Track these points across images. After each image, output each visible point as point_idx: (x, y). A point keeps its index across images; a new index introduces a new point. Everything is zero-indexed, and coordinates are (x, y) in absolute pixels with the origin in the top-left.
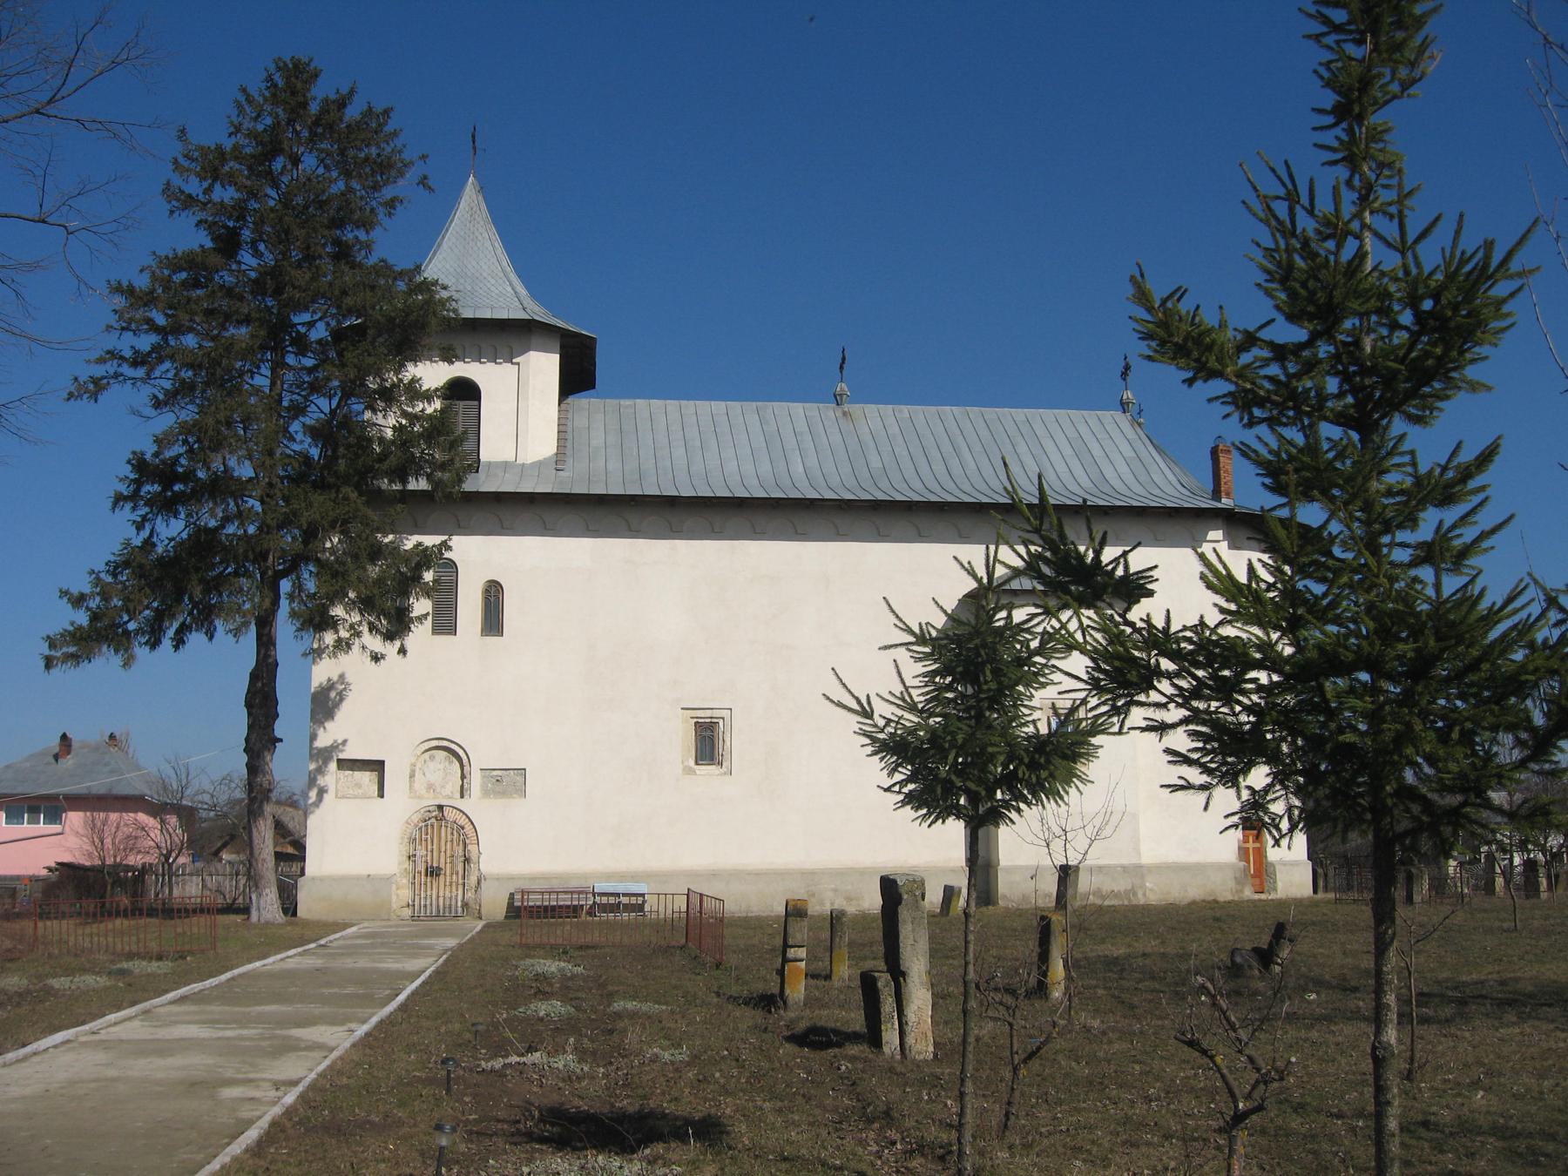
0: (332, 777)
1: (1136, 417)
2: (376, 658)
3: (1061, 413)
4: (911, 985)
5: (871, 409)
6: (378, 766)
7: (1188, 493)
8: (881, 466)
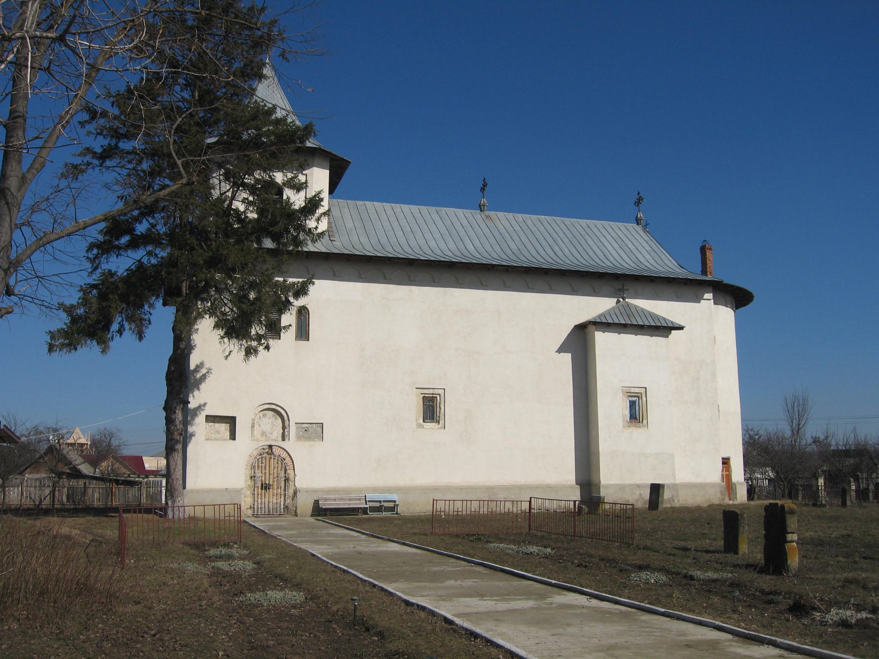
6: (231, 421)
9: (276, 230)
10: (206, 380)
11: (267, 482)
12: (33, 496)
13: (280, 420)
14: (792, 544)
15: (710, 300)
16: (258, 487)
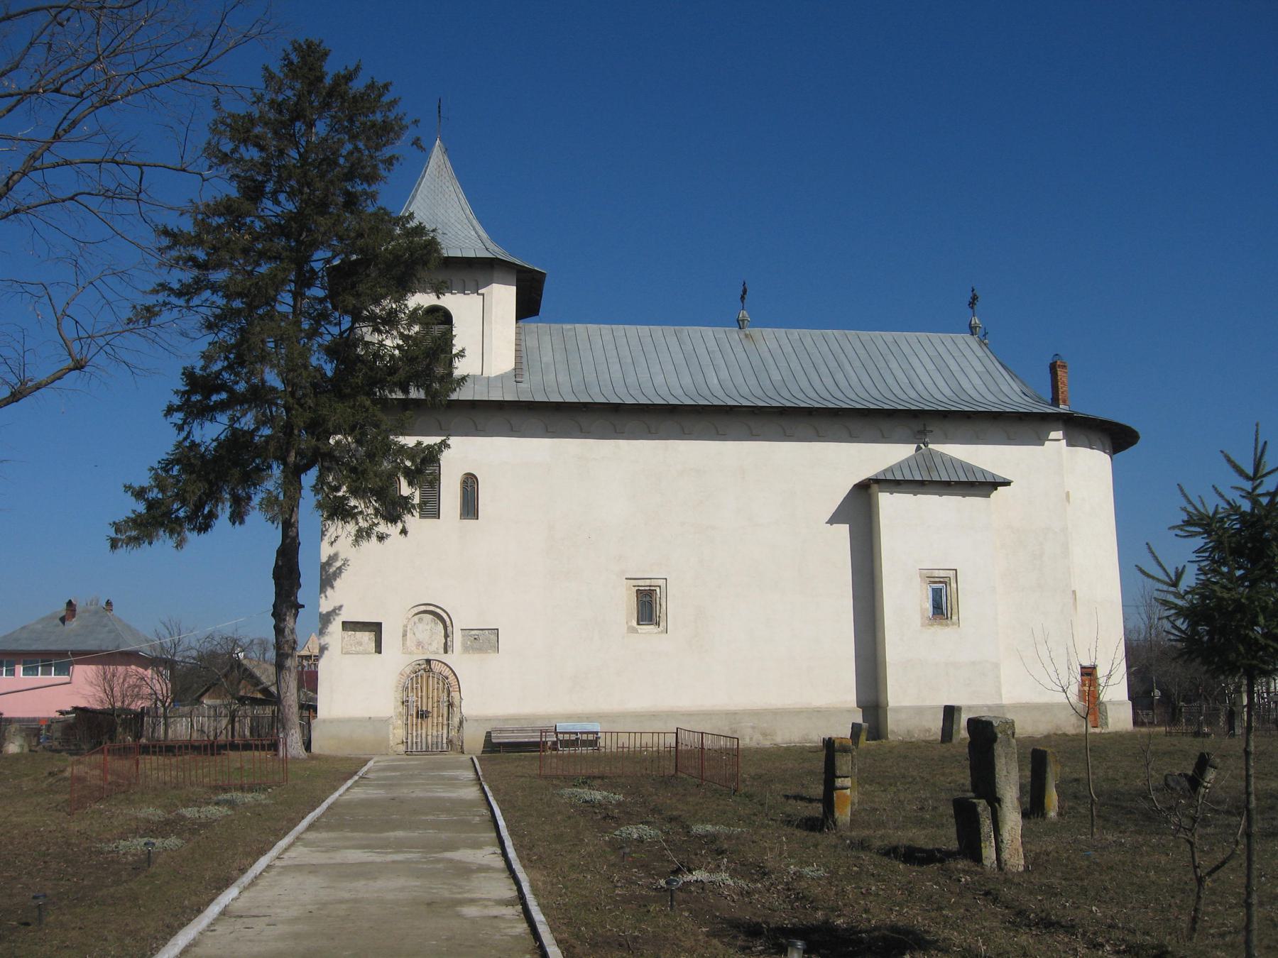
1: (983, 338)
2: (381, 538)
3: (922, 336)
5: (768, 331)
6: (376, 628)
7: (1031, 401)
8: (780, 378)
10: (343, 575)
11: (424, 709)
12: (206, 729)
13: (441, 626)
14: (845, 791)
15: (1059, 440)
16: (412, 715)
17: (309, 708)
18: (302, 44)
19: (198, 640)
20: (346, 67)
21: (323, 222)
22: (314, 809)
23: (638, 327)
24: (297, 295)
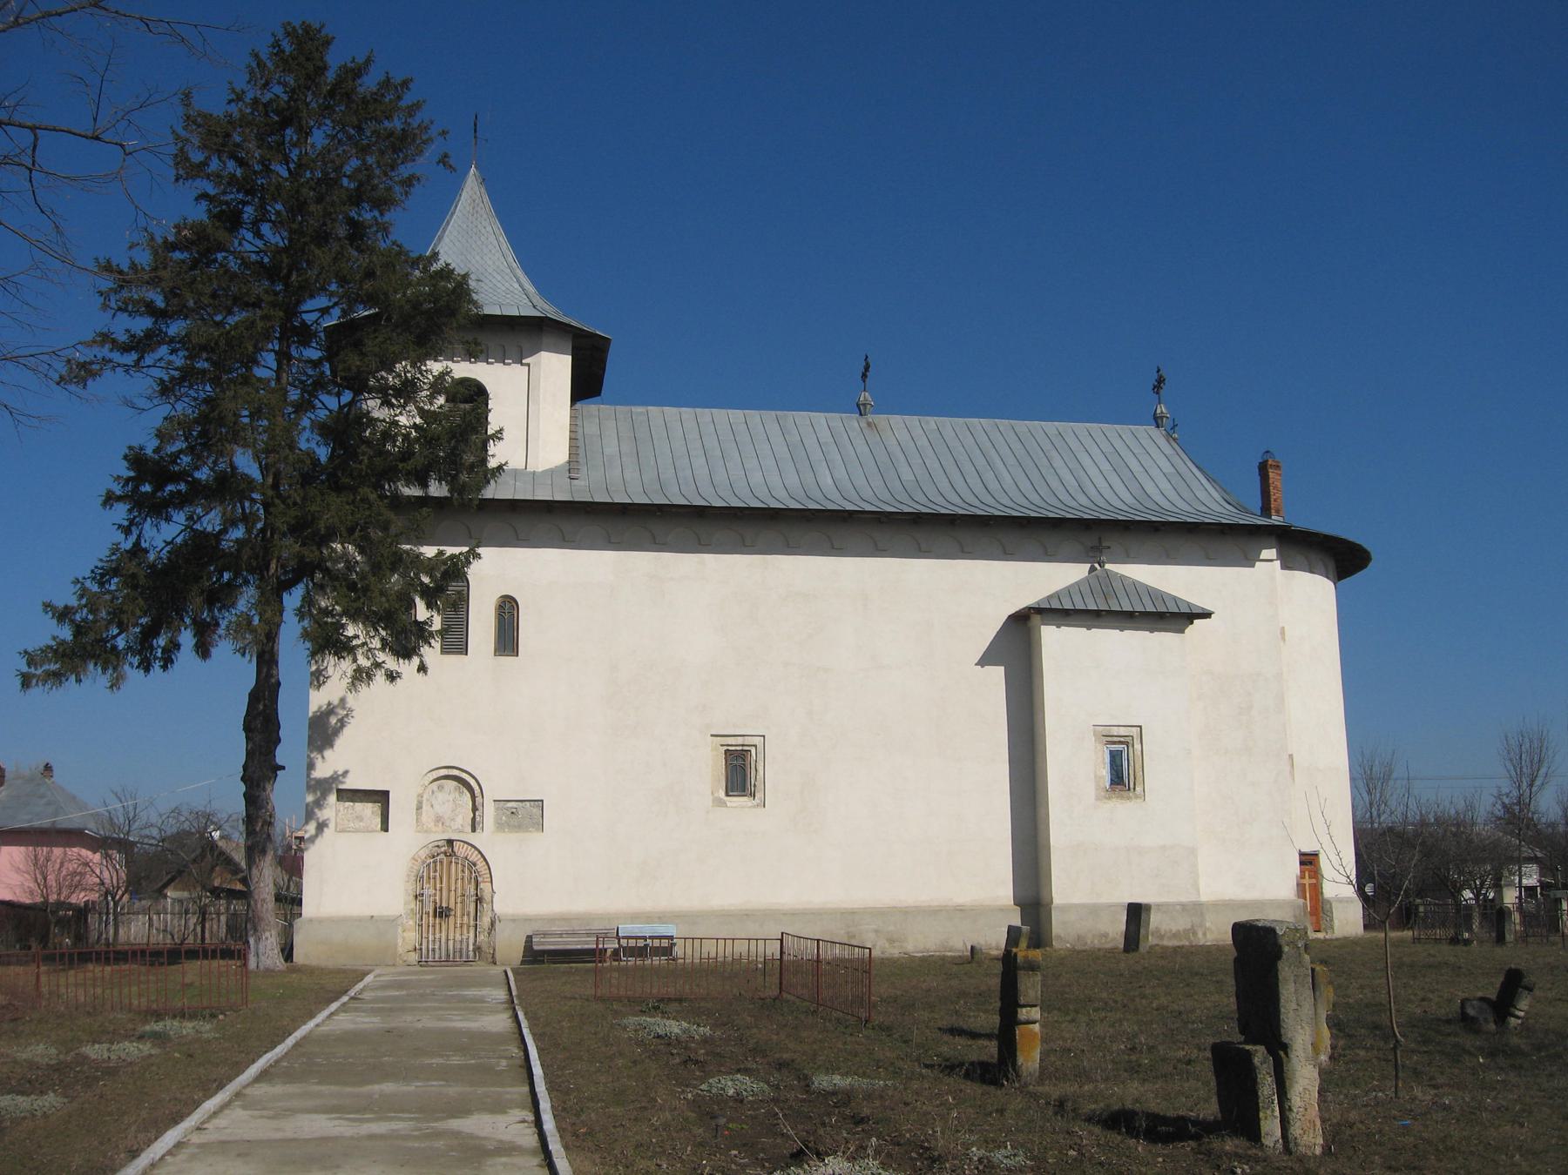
0: (332, 809)
2: (392, 677)
3: (1094, 427)
4: (1294, 1060)
5: (896, 420)
6: (381, 798)
9: (409, 468)
11: (444, 905)
14: (1031, 1026)
15: (1271, 560)
17: (290, 901)
18: (298, 27)
19: (161, 816)
20: (354, 59)
21: (323, 256)
22: (273, 1048)
23: (729, 411)
24: (283, 357)
